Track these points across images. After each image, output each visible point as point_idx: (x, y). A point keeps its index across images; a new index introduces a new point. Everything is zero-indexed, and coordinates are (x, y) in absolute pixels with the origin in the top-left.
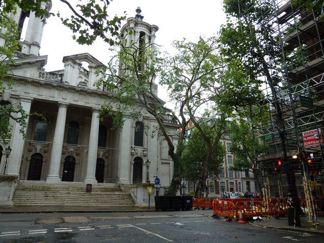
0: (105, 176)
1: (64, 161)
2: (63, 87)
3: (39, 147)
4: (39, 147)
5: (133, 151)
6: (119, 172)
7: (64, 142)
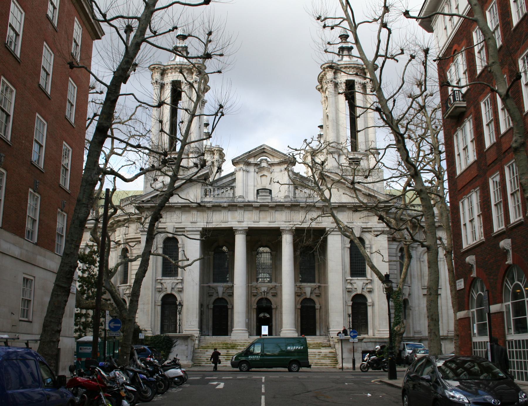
0: (318, 325)
1: (299, 306)
2: (236, 206)
3: (220, 290)
4: (308, 291)
5: (349, 286)
7: (296, 280)
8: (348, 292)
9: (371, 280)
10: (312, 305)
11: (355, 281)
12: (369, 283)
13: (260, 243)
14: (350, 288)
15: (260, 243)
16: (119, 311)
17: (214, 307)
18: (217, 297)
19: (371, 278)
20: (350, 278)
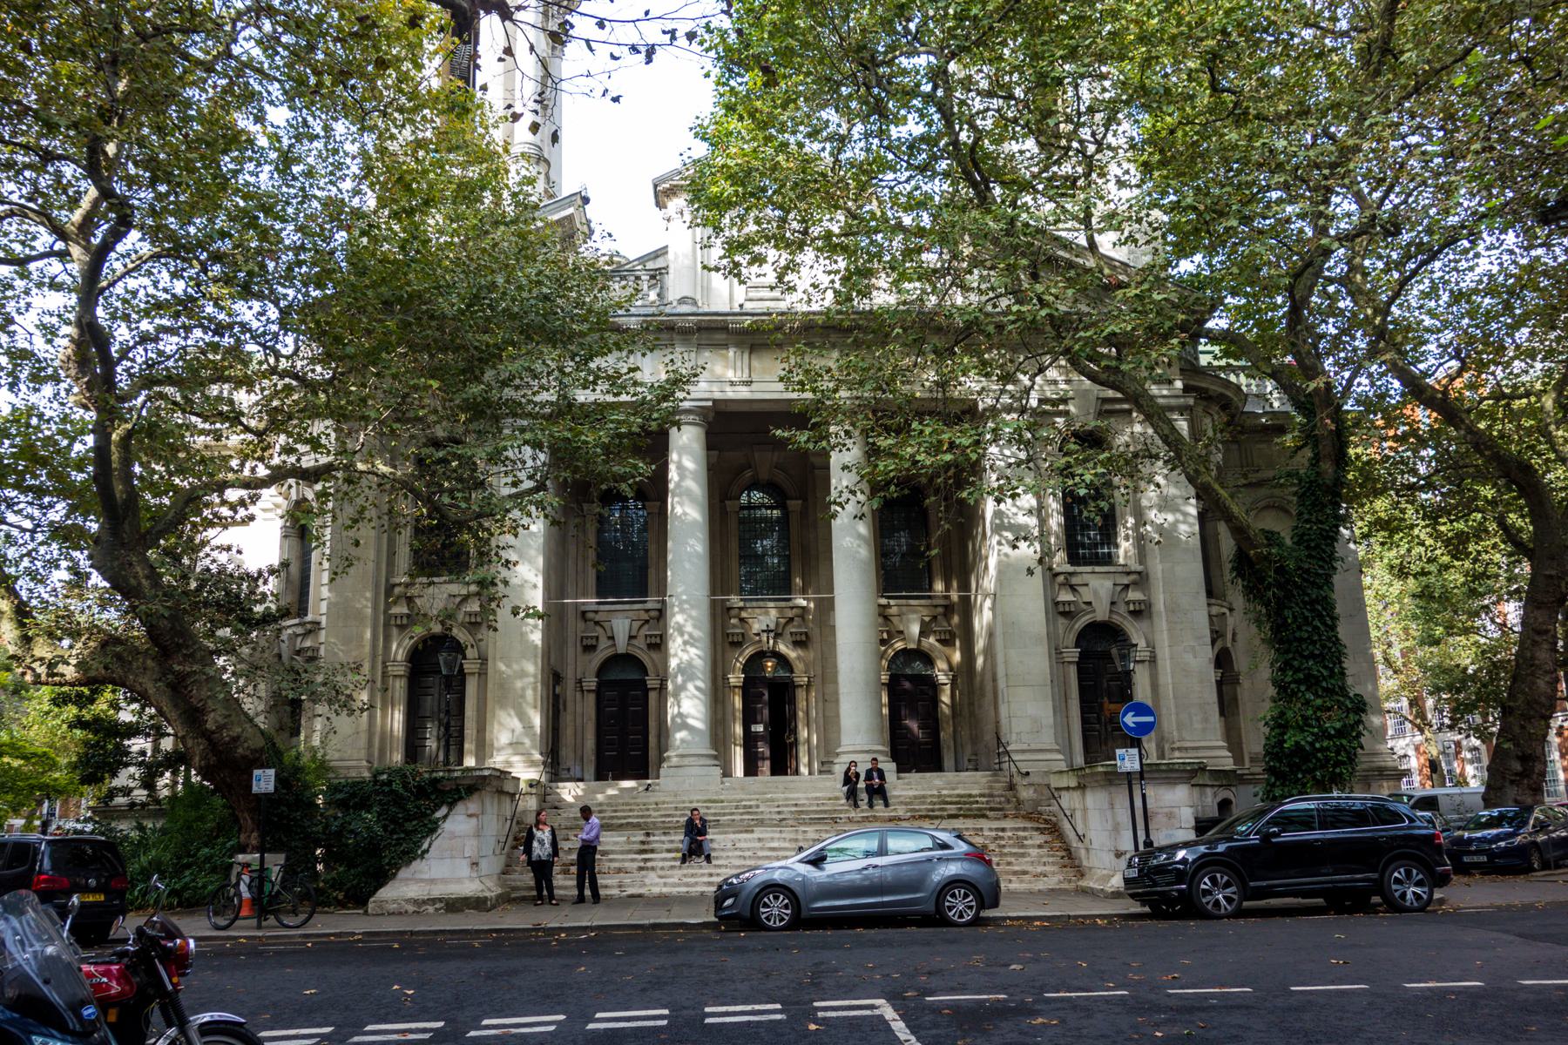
3: (621, 626)
5: (1066, 596)
6: (1003, 710)
8: (1065, 614)
9: (1139, 573)
10: (635, 676)
11: (1087, 578)
12: (1135, 583)
13: (748, 474)
14: (1069, 603)
15: (748, 474)
16: (1510, 689)
17: (599, 685)
18: (609, 652)
19: (1139, 568)
20: (1070, 568)
